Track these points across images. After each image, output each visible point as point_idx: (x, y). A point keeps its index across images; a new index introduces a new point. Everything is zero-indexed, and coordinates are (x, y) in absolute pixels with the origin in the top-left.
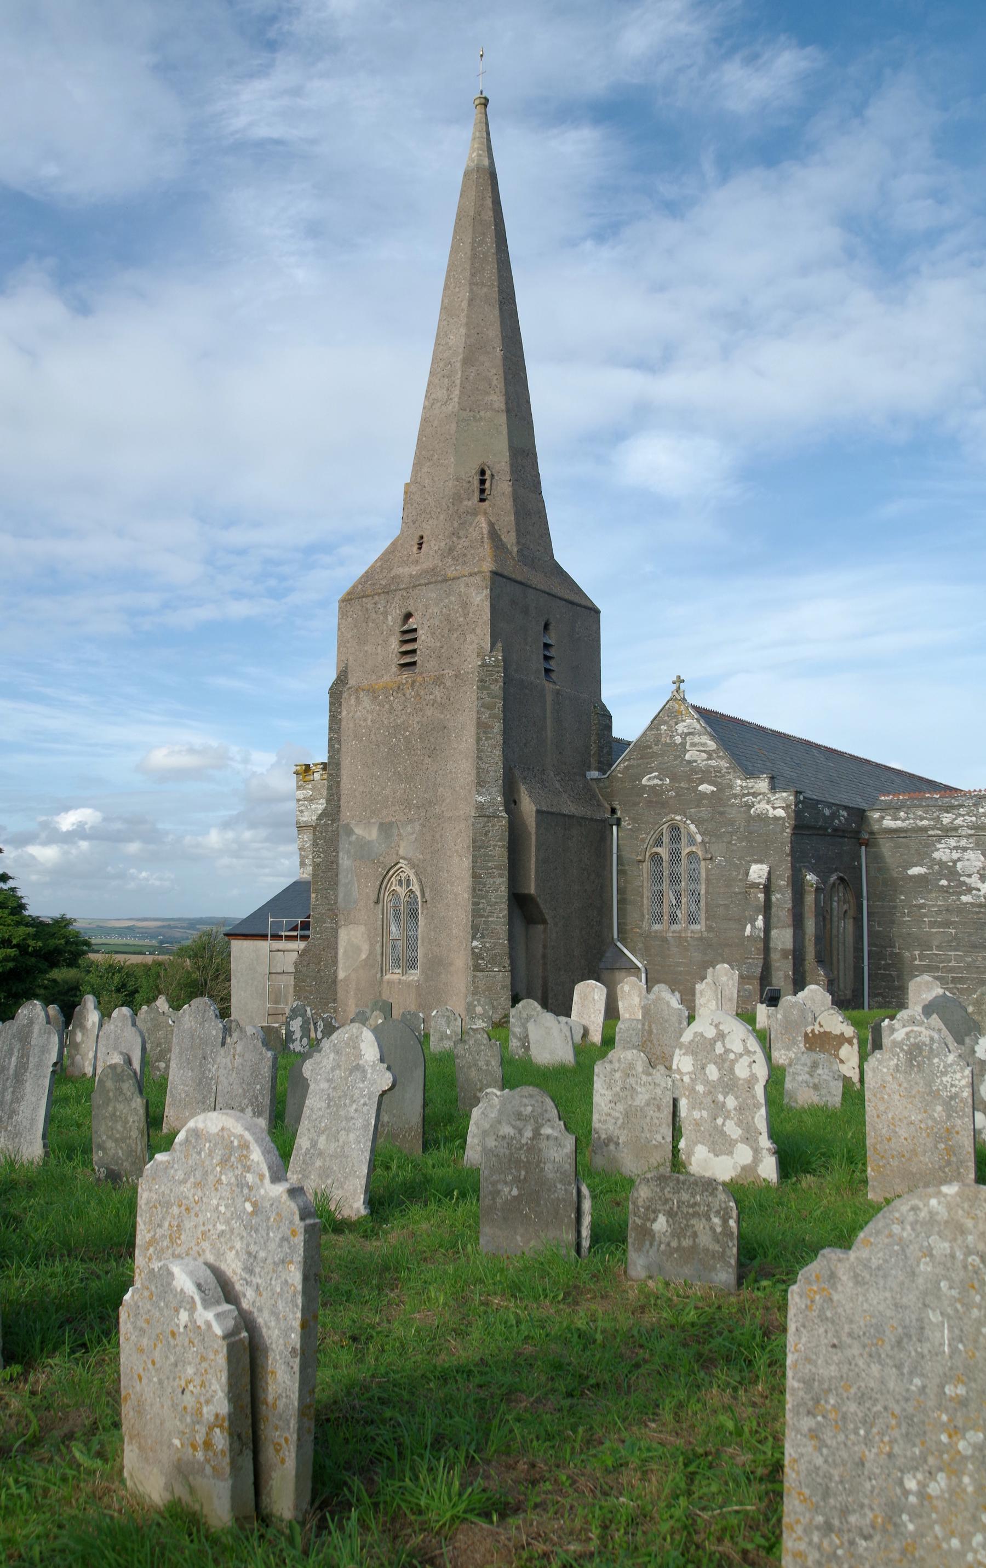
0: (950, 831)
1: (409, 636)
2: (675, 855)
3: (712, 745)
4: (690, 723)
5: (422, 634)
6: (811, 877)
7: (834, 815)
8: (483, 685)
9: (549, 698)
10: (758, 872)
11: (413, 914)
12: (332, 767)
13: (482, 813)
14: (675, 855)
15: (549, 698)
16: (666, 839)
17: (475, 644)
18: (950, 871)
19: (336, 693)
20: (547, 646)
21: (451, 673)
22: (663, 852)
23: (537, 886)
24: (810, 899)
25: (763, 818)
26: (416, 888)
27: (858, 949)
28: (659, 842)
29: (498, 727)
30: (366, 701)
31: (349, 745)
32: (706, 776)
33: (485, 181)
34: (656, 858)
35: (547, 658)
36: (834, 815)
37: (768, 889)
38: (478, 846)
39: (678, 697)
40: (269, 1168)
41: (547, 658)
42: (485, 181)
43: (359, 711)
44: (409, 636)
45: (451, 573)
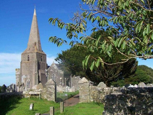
2: (54, 77)
3: (56, 67)
4: (55, 65)
6: (65, 79)
8: (36, 62)
10: (61, 78)
11: (29, 83)
12: (21, 69)
13: (36, 74)
14: (54, 77)
16: (53, 75)
17: (35, 59)
19: (21, 63)
20: (41, 58)
21: (76, 43)
22: (52, 77)
23: (41, 79)
24: (65, 81)
25: (61, 74)
26: (29, 80)
28: (52, 76)
29: (37, 66)
30: (24, 63)
31: (23, 67)
32: (56, 70)
35: (41, 60)
37: (62, 80)
38: (35, 77)
40: (30, 29)
41: (41, 60)
43: (24, 64)
45: (32, 52)
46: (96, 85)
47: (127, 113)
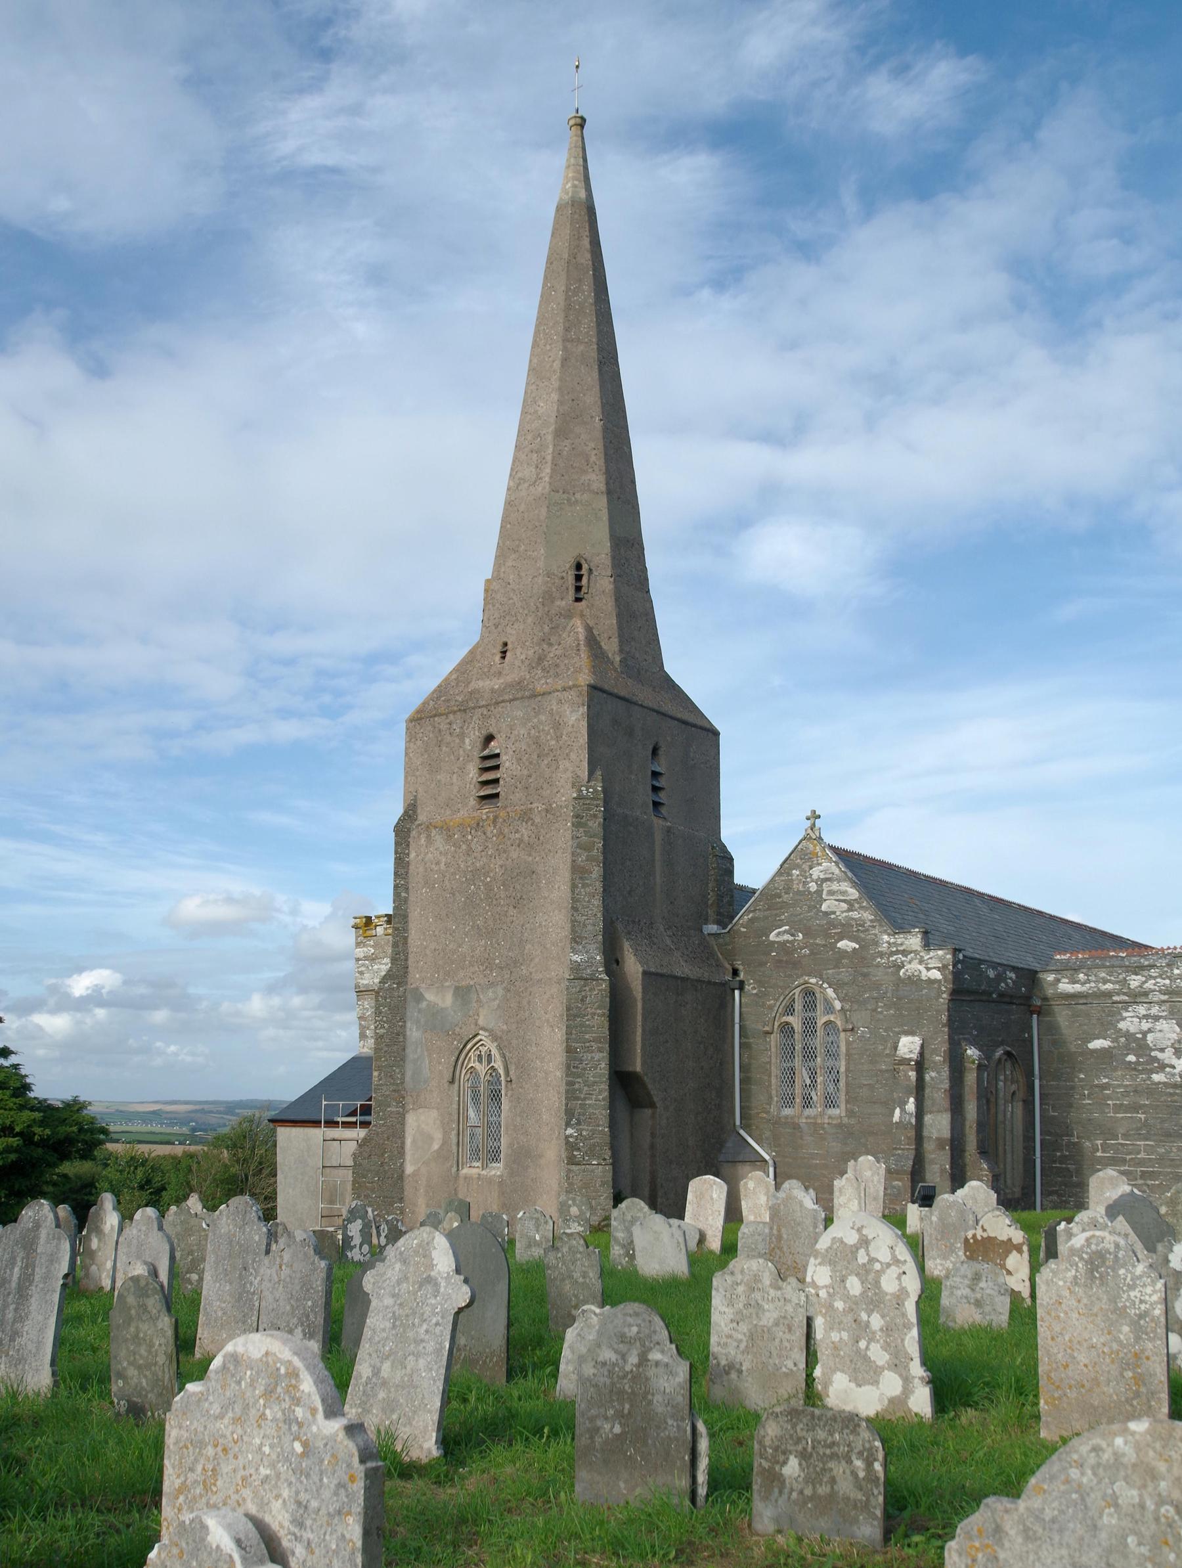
0: (1139, 996)
1: (490, 763)
2: (809, 1026)
3: (853, 893)
4: (827, 866)
5: (506, 761)
6: (972, 1052)
7: (1000, 978)
9: (658, 837)
10: (909, 1046)
11: (496, 1096)
12: (397, 920)
13: (578, 975)
14: (809, 1026)
15: (658, 837)
16: (798, 1006)
18: (1138, 1044)
20: (655, 775)
22: (795, 1021)
23: (644, 1063)
24: (971, 1078)
25: (914, 981)
26: (498, 1064)
27: (1029, 1138)
28: (790, 1010)
29: (597, 872)
30: (439, 840)
31: (418, 895)
32: (847, 930)
33: (582, 217)
34: (787, 1029)
35: (655, 789)
36: (1000, 978)
37: (920, 1066)
38: (573, 1015)
39: (812, 836)
41: (655, 789)
42: (582, 217)
43: (430, 853)
44: (490, 763)
45: (540, 687)
46: (930, 1206)
47: (757, 1279)
